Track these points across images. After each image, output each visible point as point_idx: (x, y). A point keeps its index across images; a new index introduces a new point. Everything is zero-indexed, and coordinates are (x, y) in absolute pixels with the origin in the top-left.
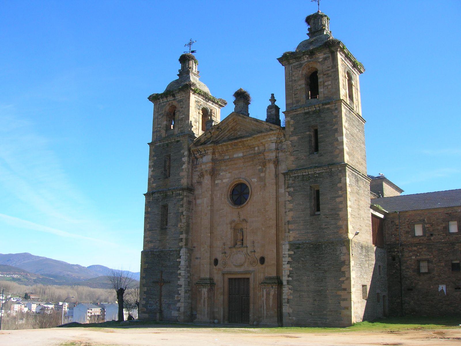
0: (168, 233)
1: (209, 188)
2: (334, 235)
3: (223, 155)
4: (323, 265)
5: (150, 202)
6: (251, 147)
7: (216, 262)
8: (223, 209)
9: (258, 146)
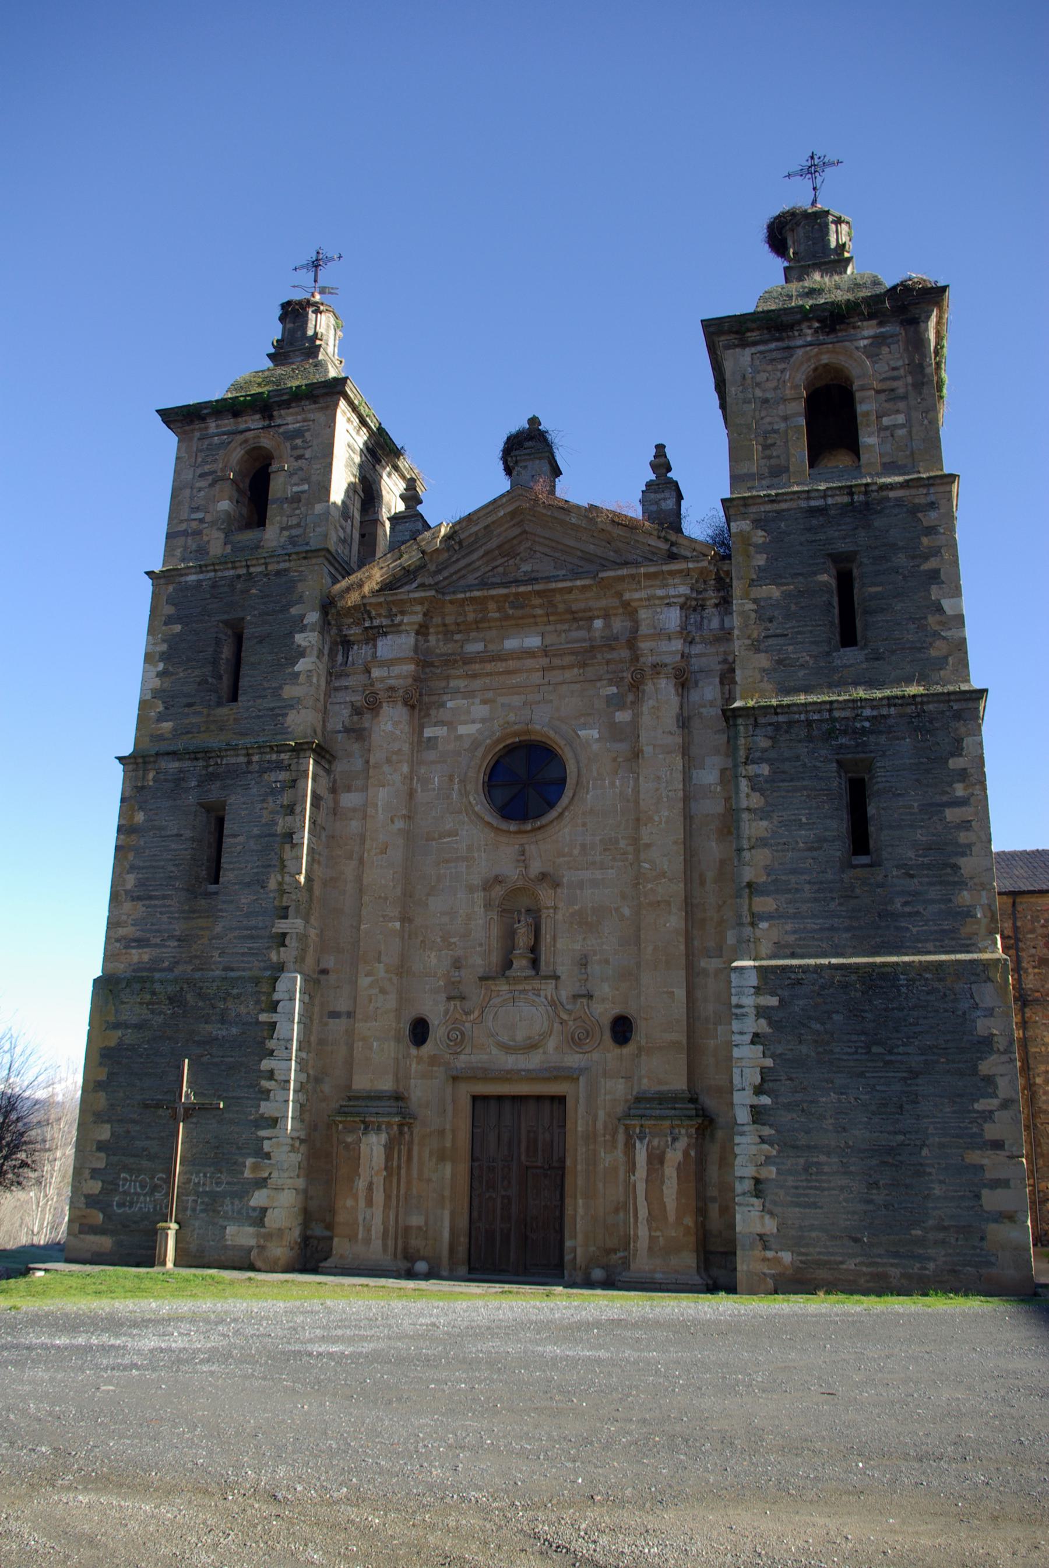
0: (221, 910)
1: (400, 750)
2: (942, 941)
3: (457, 637)
4: (901, 1050)
5: (143, 788)
6: (576, 615)
7: (420, 1031)
8: (453, 833)
9: (606, 616)
